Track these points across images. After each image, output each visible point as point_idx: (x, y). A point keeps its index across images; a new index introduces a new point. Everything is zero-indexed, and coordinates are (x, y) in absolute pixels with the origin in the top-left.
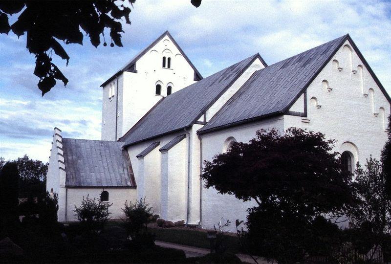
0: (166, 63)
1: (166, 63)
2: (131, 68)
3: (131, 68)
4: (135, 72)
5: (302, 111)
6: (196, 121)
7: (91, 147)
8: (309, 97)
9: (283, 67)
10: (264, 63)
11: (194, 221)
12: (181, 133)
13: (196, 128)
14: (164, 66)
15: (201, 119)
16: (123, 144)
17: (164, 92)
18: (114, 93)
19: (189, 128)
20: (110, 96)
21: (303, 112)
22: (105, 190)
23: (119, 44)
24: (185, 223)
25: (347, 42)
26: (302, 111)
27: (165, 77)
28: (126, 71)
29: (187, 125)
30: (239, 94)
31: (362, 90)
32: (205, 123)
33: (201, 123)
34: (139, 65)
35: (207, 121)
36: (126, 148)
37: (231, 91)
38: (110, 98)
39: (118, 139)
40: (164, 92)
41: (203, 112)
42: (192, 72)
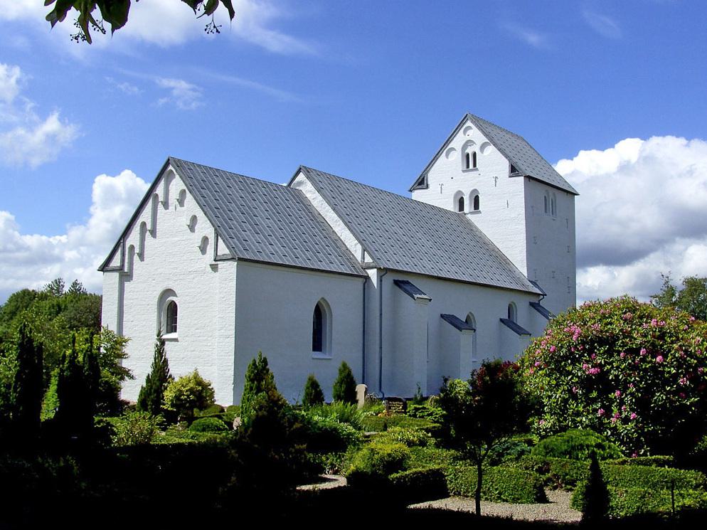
2: (514, 171)
5: (118, 264)
34: (432, 178)
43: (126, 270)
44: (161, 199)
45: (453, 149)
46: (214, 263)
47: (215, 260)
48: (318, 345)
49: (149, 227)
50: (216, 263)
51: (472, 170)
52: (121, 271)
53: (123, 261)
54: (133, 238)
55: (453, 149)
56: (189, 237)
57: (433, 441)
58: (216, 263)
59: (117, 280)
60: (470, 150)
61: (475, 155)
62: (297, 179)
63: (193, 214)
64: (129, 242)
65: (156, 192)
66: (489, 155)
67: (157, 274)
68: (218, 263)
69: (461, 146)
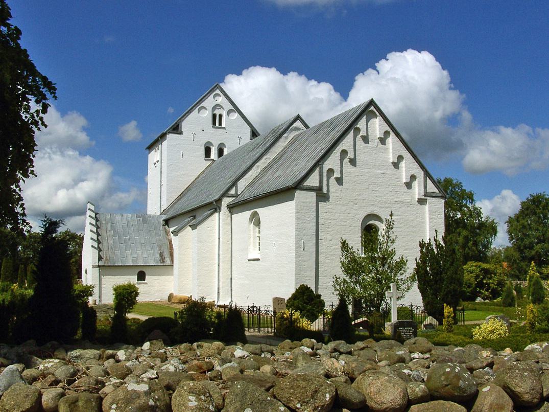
0: (216, 120)
1: (216, 120)
2: (176, 129)
3: (176, 129)
4: (181, 133)
5: (317, 184)
6: (225, 194)
7: (128, 222)
8: (325, 170)
9: (315, 133)
10: (306, 126)
11: (314, 330)
12: (214, 206)
13: (226, 201)
14: (214, 123)
15: (233, 191)
16: (164, 217)
17: (214, 154)
18: (159, 159)
19: (219, 201)
20: (155, 161)
21: (318, 185)
22: (472, 340)
23: (36, 176)
24: (215, 304)
25: (372, 108)
26: (317, 184)
27: (216, 137)
28: (170, 133)
29: (216, 198)
30: (276, 160)
31: (392, 158)
32: (236, 196)
33: (232, 196)
34: (184, 126)
35: (239, 193)
36: (167, 222)
37: (266, 159)
38: (155, 164)
39: (162, 211)
40: (214, 154)
41: (234, 184)
42: (249, 130)
43: (325, 191)
44: (363, 133)
45: (204, 108)
46: (423, 197)
47: (425, 196)
48: (259, 250)
49: (351, 155)
50: (426, 198)
51: (217, 128)
52: (318, 192)
53: (321, 181)
54: (332, 162)
55: (204, 108)
56: (393, 172)
57: (293, 311)
58: (426, 198)
59: (314, 199)
60: (217, 112)
61: (221, 116)
62: (295, 125)
63: (399, 154)
64: (327, 165)
65: (358, 126)
66: (234, 119)
67: (360, 200)
68: (428, 198)
69: (212, 107)
